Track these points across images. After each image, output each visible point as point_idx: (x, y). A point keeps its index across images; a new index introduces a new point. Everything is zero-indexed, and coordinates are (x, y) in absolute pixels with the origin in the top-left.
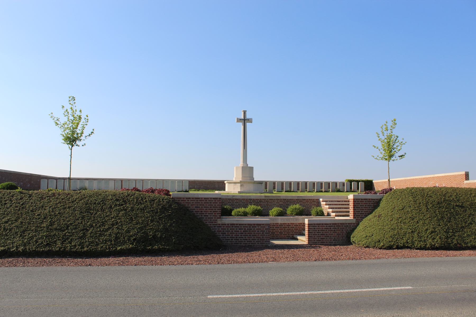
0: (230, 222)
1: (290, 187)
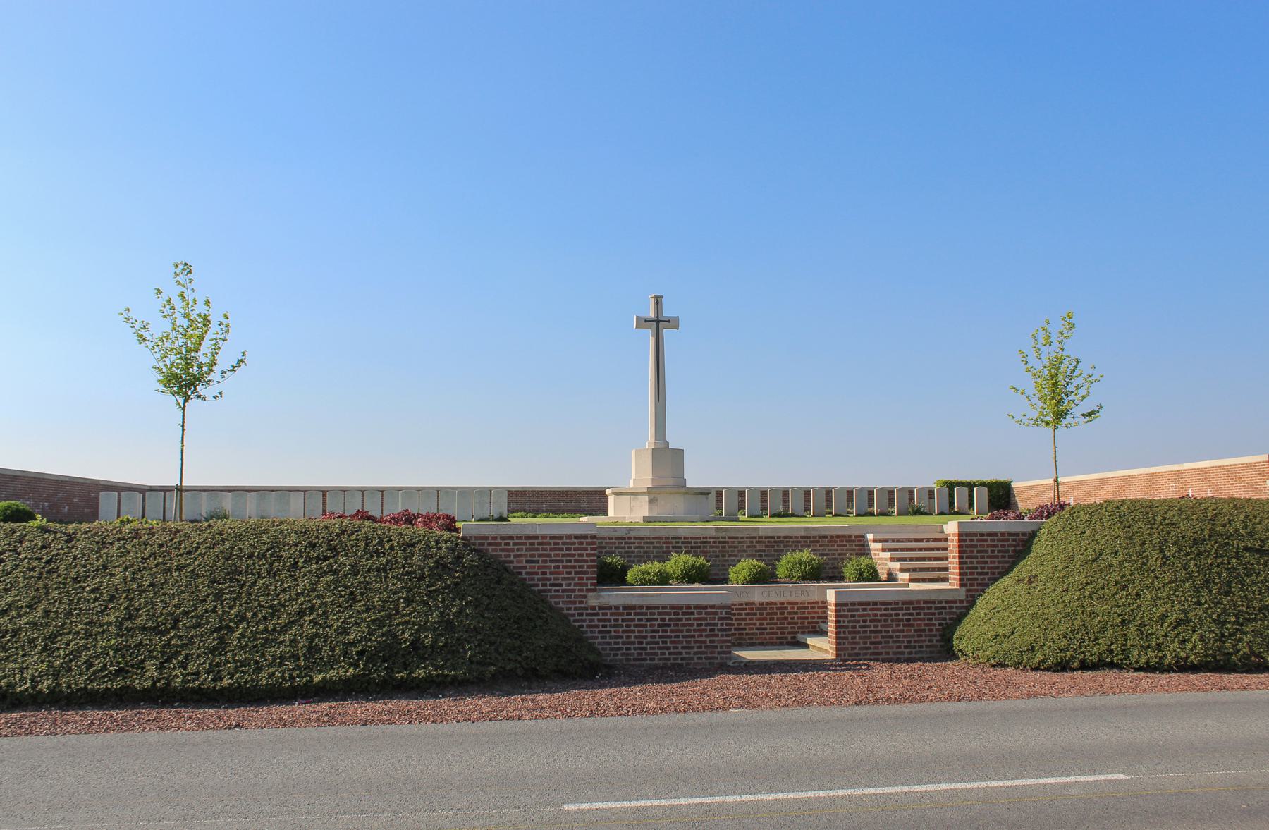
0: (621, 602)
1: (786, 504)
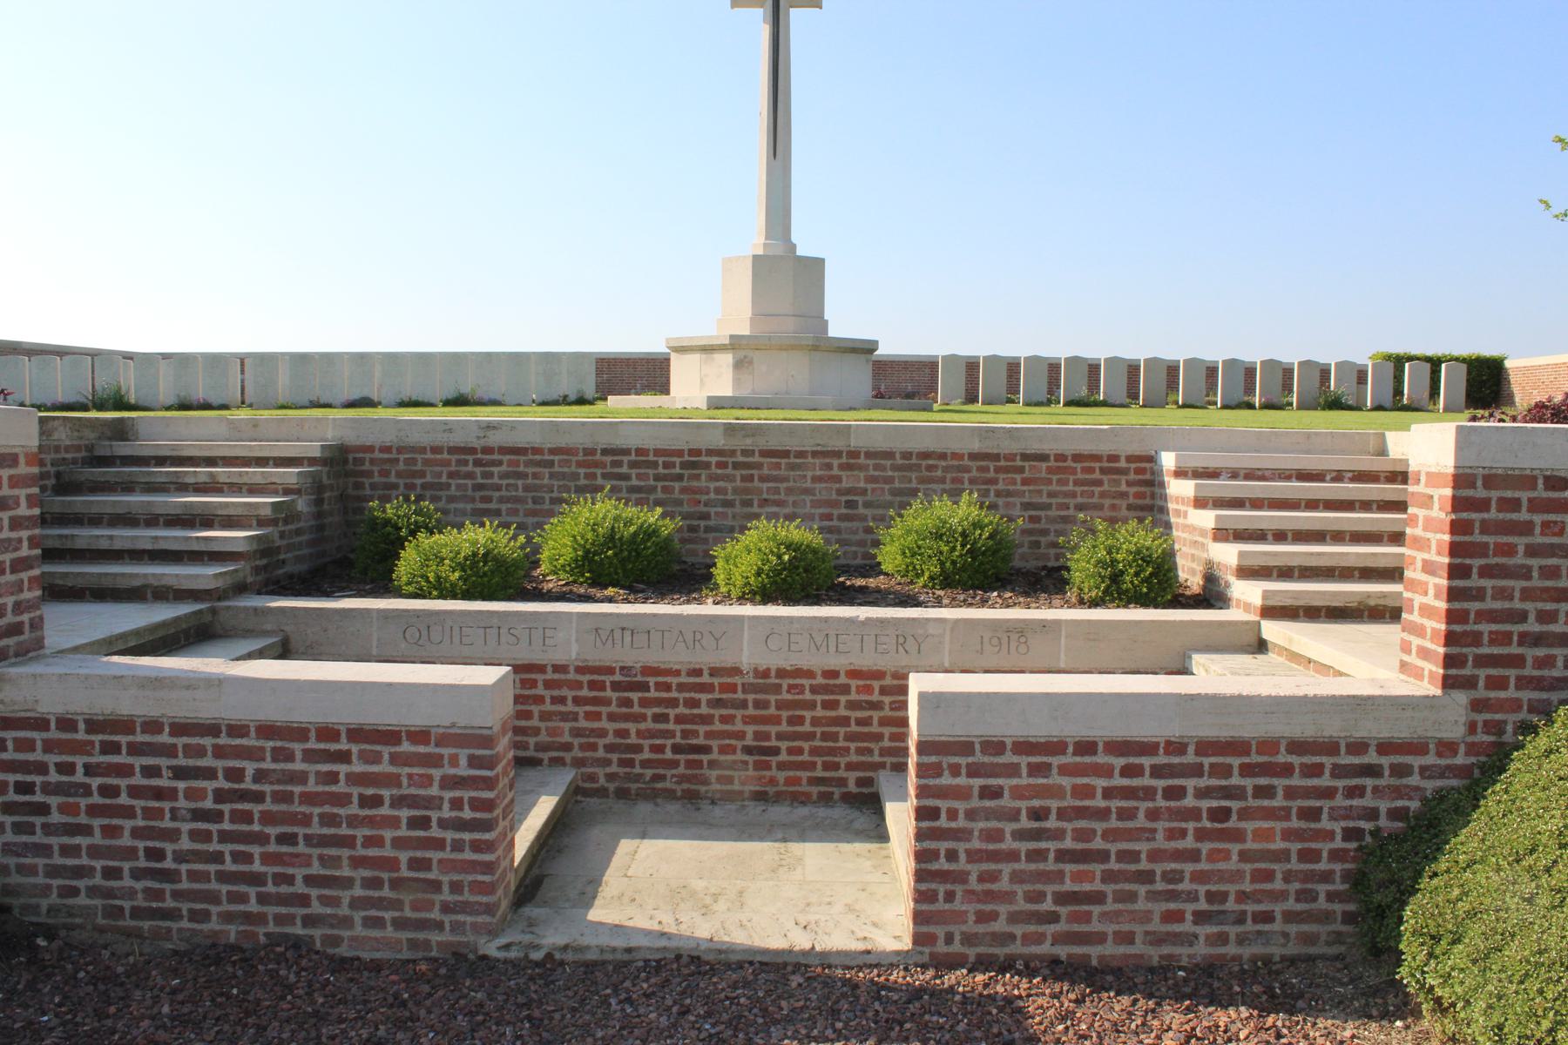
0: (81, 703)
1: (1093, 384)
